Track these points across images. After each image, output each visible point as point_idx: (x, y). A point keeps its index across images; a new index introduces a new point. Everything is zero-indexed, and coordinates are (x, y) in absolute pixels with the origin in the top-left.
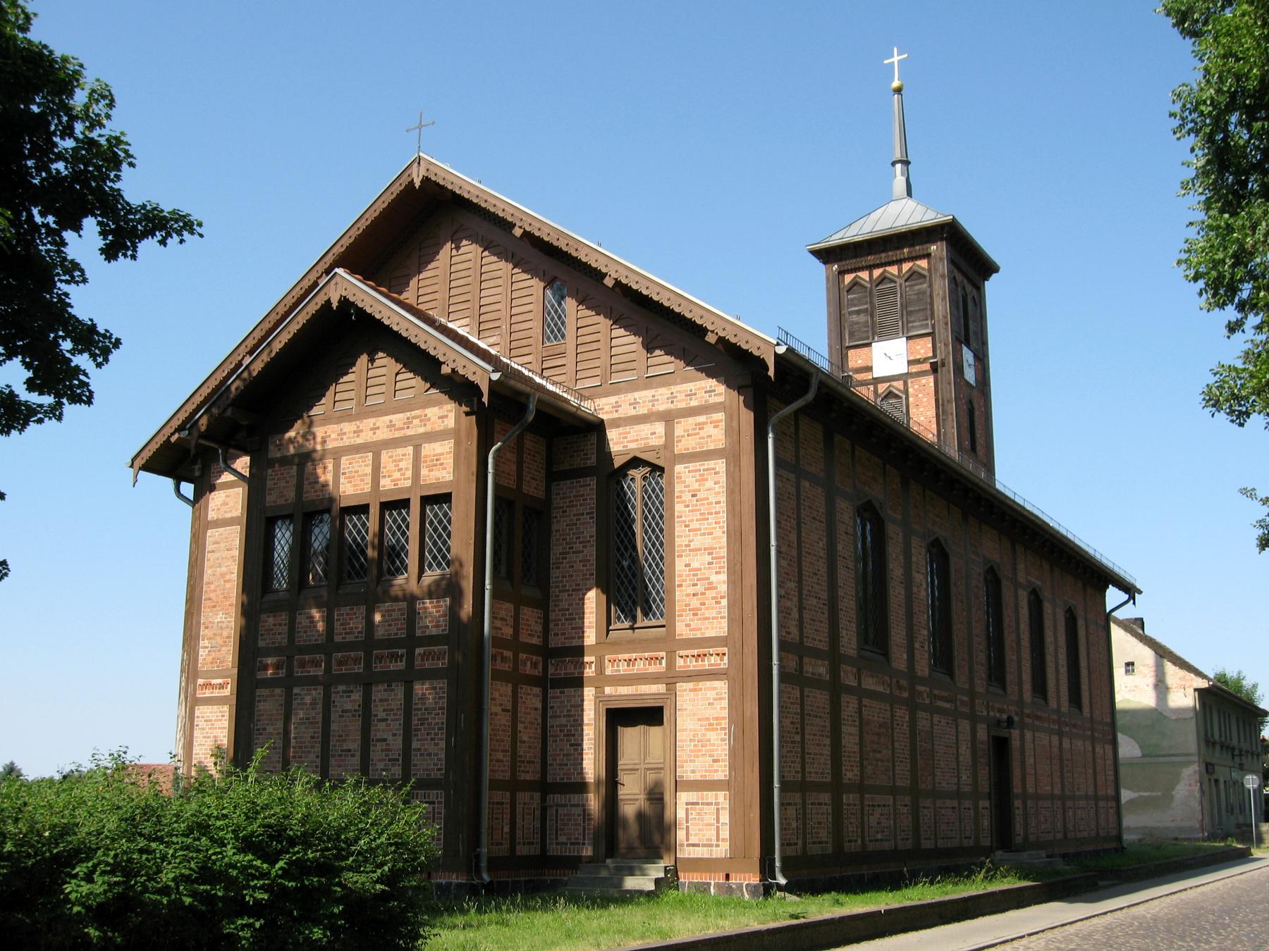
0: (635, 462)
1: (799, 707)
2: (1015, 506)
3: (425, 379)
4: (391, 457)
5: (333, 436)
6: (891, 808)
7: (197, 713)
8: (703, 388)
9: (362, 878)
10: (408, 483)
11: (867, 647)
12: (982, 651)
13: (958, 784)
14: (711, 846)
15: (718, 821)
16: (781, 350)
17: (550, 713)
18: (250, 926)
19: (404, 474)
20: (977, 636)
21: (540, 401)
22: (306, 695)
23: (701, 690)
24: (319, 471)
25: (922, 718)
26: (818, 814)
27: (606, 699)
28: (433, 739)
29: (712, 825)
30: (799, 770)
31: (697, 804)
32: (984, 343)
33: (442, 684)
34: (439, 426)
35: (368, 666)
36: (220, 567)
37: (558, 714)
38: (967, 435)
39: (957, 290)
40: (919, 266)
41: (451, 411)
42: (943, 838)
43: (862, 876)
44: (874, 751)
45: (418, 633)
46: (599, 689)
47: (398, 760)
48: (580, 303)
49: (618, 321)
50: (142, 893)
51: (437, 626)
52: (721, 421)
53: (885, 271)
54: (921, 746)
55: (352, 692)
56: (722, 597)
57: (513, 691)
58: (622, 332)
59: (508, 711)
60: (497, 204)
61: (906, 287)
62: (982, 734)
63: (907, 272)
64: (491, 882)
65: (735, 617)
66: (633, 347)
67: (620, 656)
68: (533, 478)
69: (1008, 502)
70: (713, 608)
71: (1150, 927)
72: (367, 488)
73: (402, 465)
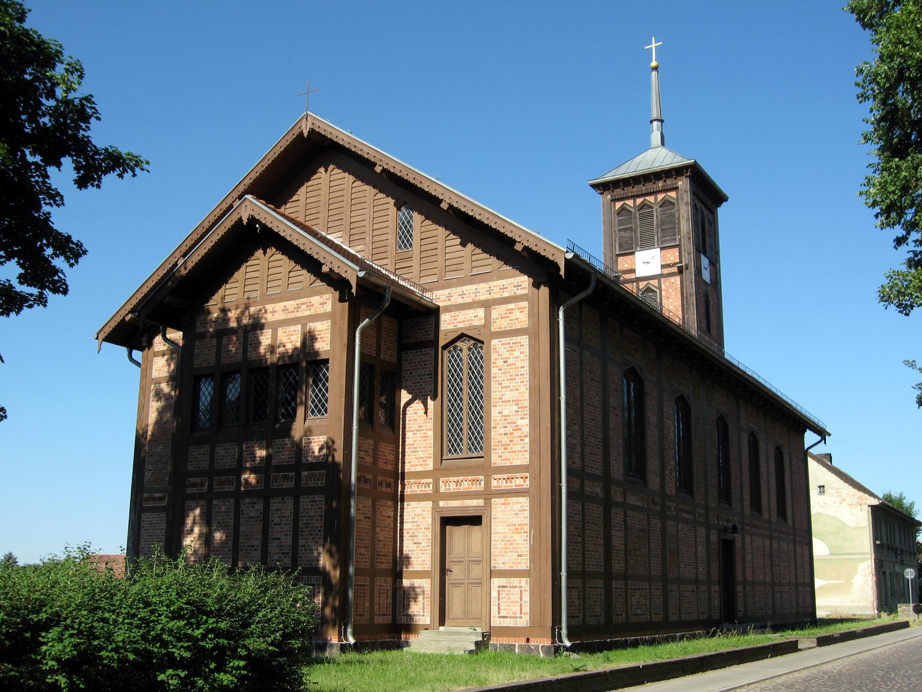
0: (462, 336)
1: (581, 516)
2: (739, 371)
7: (143, 518)
8: (512, 284)
11: (631, 474)
14: (516, 617)
15: (521, 600)
16: (570, 256)
20: (711, 466)
21: (393, 293)
22: (222, 505)
23: (509, 504)
26: (594, 595)
27: (440, 510)
28: (314, 538)
29: (517, 602)
31: (506, 587)
32: (716, 253)
34: (321, 310)
40: (670, 196)
41: (329, 299)
42: (685, 613)
44: (635, 550)
47: (288, 553)
55: (255, 503)
59: (368, 518)
62: (714, 537)
63: (660, 201)
65: (534, 451)
68: (387, 349)
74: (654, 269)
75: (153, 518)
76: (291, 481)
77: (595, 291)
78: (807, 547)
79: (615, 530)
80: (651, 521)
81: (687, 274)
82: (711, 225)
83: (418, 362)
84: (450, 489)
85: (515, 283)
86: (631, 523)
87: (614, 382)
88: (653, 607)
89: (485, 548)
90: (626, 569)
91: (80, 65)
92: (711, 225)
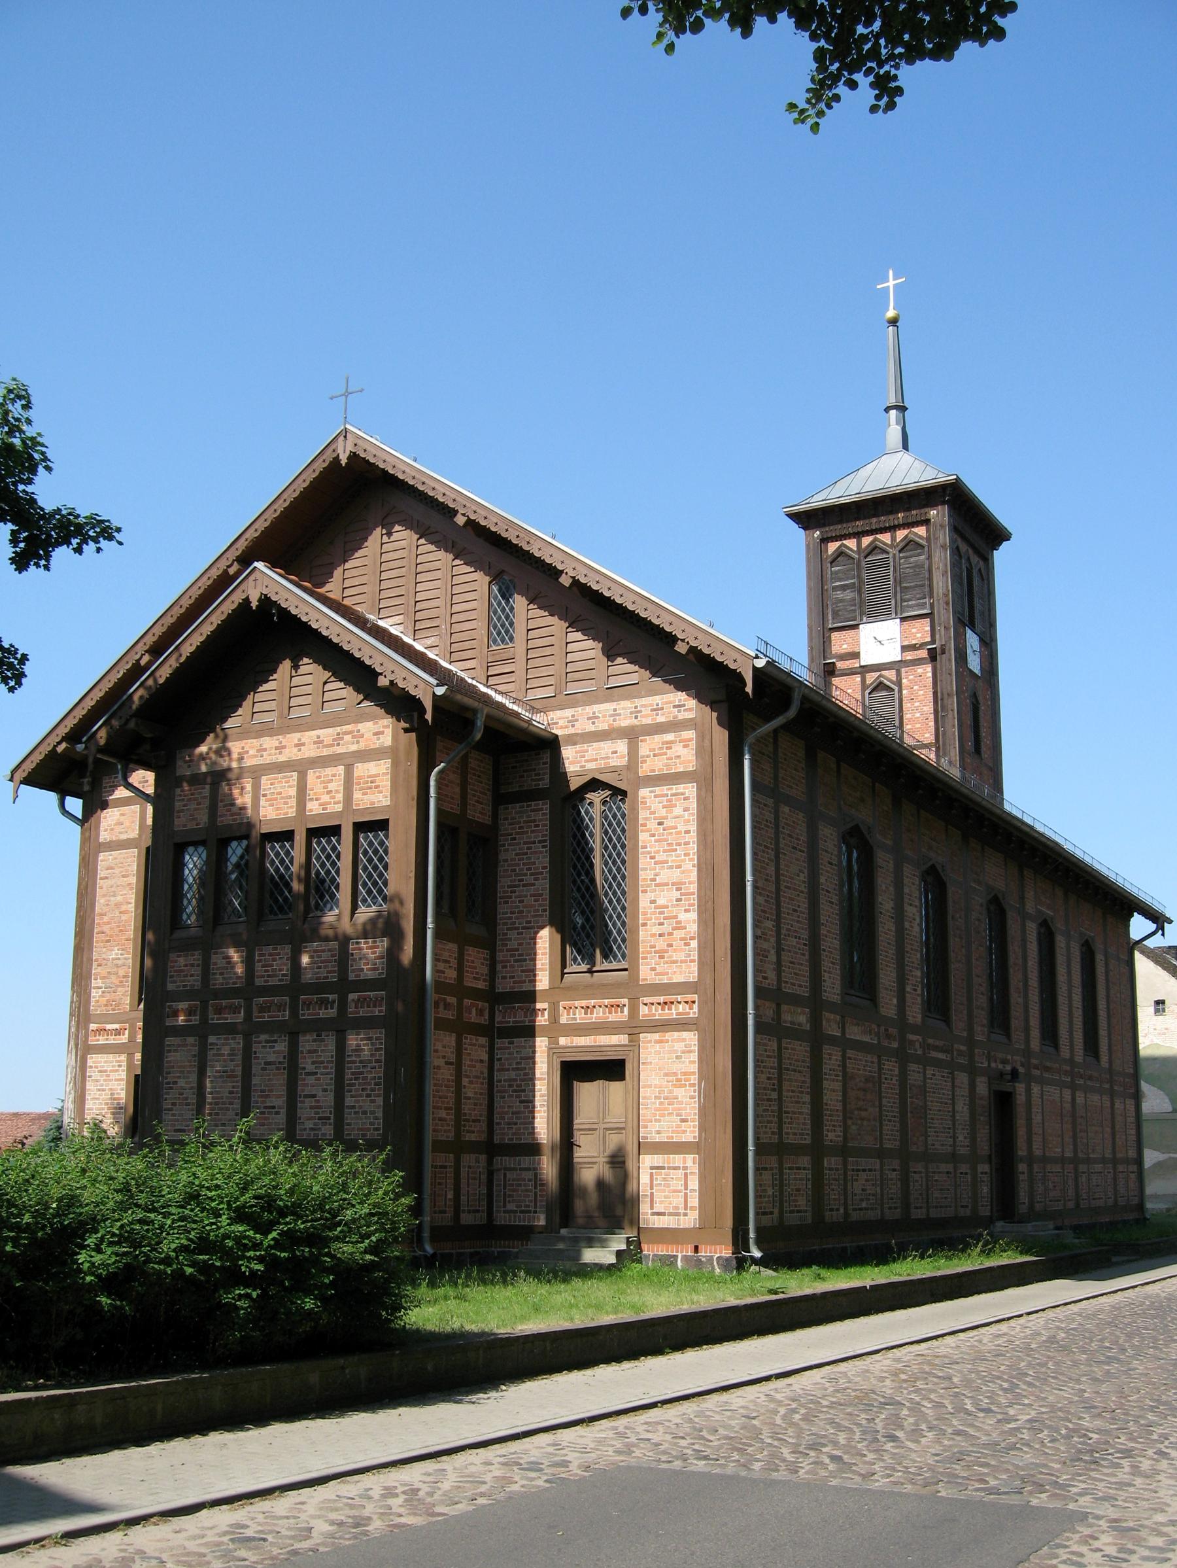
0: (594, 784)
1: (776, 1060)
2: (1023, 827)
3: (358, 691)
4: (319, 777)
5: (252, 752)
6: (878, 1173)
7: (90, 1062)
8: (670, 702)
9: (348, 1248)
10: (339, 808)
11: (852, 992)
12: (982, 994)
13: (954, 1145)
14: (678, 1214)
15: (686, 1188)
16: (760, 663)
17: (497, 1065)
18: (248, 1296)
19: (334, 798)
20: (978, 976)
21: (488, 716)
22: (223, 1045)
23: (667, 1041)
24: (236, 792)
25: (914, 1071)
26: (795, 1179)
27: (561, 1050)
28: (368, 1096)
29: (680, 1191)
30: (776, 1130)
31: (663, 1168)
32: (991, 625)
33: (379, 1034)
34: (375, 743)
35: (294, 1013)
36: (114, 896)
37: (507, 1067)
38: (970, 736)
39: (961, 563)
40: (916, 534)
41: (388, 727)
42: (936, 1207)
43: (844, 1249)
44: (860, 1109)
45: (352, 977)
46: (553, 1039)
47: (329, 1118)
48: (531, 601)
49: (575, 623)
50: (145, 1262)
51: (374, 969)
52: (691, 740)
53: (876, 539)
54: (912, 1103)
55: (275, 1041)
56: (692, 938)
57: (457, 1043)
58: (579, 636)
59: (451, 1063)
60: (437, 487)
61: (900, 558)
62: (982, 1088)
63: (901, 541)
64: (434, 1255)
65: (706, 962)
66: (592, 654)
67: (577, 1003)
68: (478, 802)
69: (1016, 822)
70: (681, 950)
71: (1162, 1306)
72: (292, 812)
73: (332, 786)
74: (892, 653)
75: (106, 1062)
76: (332, 1008)
77: (801, 711)
78: (1132, 1102)
79: (827, 1079)
80: (884, 1064)
81: (944, 661)
82: (983, 580)
83: (525, 822)
84: (575, 1019)
85: (675, 701)
86: (853, 1068)
87: (826, 851)
88: (885, 1196)
89: (631, 1109)
90: (845, 1138)
91: (26, 390)
92: (983, 579)
